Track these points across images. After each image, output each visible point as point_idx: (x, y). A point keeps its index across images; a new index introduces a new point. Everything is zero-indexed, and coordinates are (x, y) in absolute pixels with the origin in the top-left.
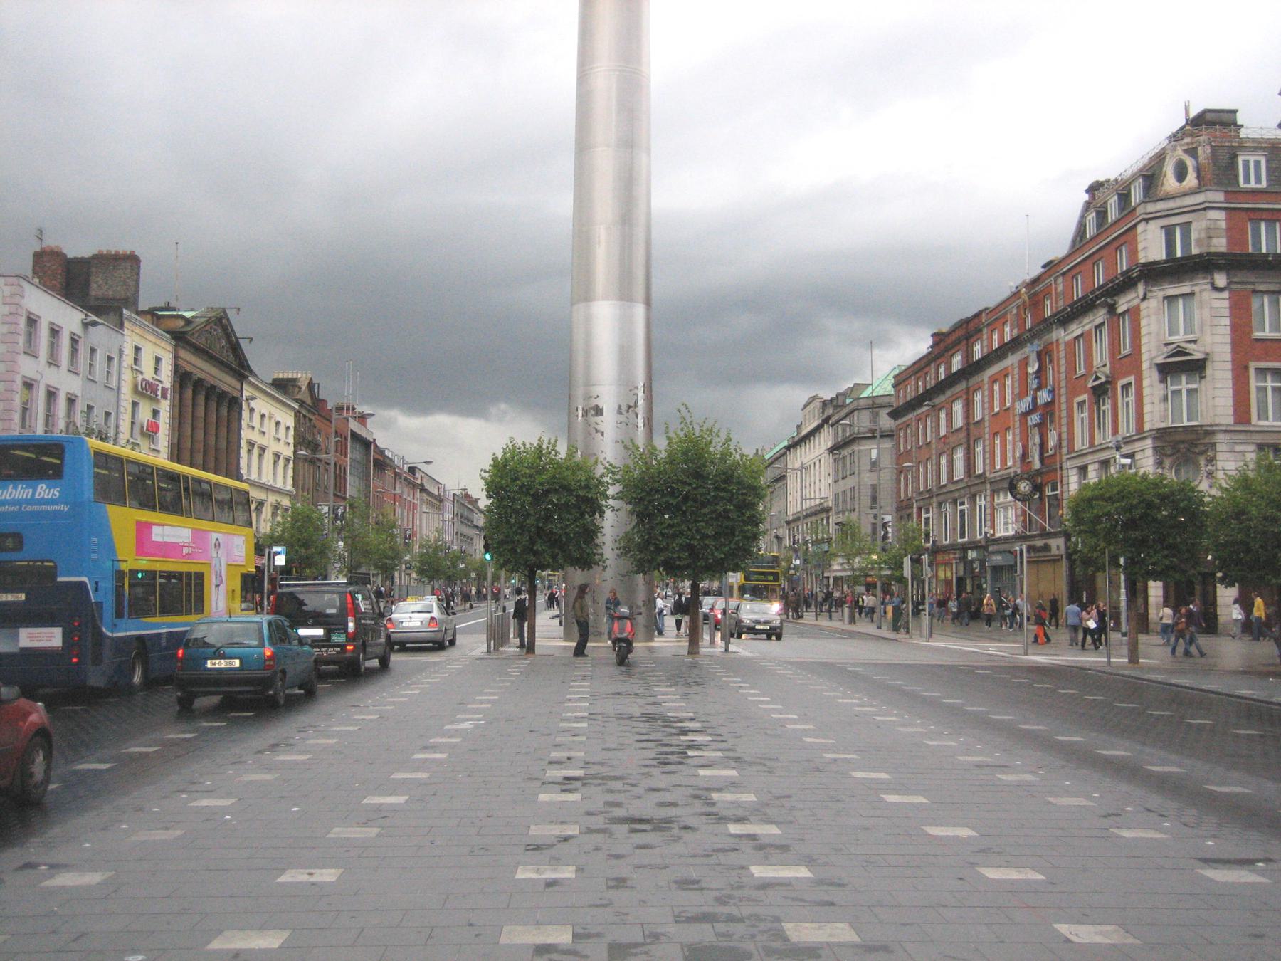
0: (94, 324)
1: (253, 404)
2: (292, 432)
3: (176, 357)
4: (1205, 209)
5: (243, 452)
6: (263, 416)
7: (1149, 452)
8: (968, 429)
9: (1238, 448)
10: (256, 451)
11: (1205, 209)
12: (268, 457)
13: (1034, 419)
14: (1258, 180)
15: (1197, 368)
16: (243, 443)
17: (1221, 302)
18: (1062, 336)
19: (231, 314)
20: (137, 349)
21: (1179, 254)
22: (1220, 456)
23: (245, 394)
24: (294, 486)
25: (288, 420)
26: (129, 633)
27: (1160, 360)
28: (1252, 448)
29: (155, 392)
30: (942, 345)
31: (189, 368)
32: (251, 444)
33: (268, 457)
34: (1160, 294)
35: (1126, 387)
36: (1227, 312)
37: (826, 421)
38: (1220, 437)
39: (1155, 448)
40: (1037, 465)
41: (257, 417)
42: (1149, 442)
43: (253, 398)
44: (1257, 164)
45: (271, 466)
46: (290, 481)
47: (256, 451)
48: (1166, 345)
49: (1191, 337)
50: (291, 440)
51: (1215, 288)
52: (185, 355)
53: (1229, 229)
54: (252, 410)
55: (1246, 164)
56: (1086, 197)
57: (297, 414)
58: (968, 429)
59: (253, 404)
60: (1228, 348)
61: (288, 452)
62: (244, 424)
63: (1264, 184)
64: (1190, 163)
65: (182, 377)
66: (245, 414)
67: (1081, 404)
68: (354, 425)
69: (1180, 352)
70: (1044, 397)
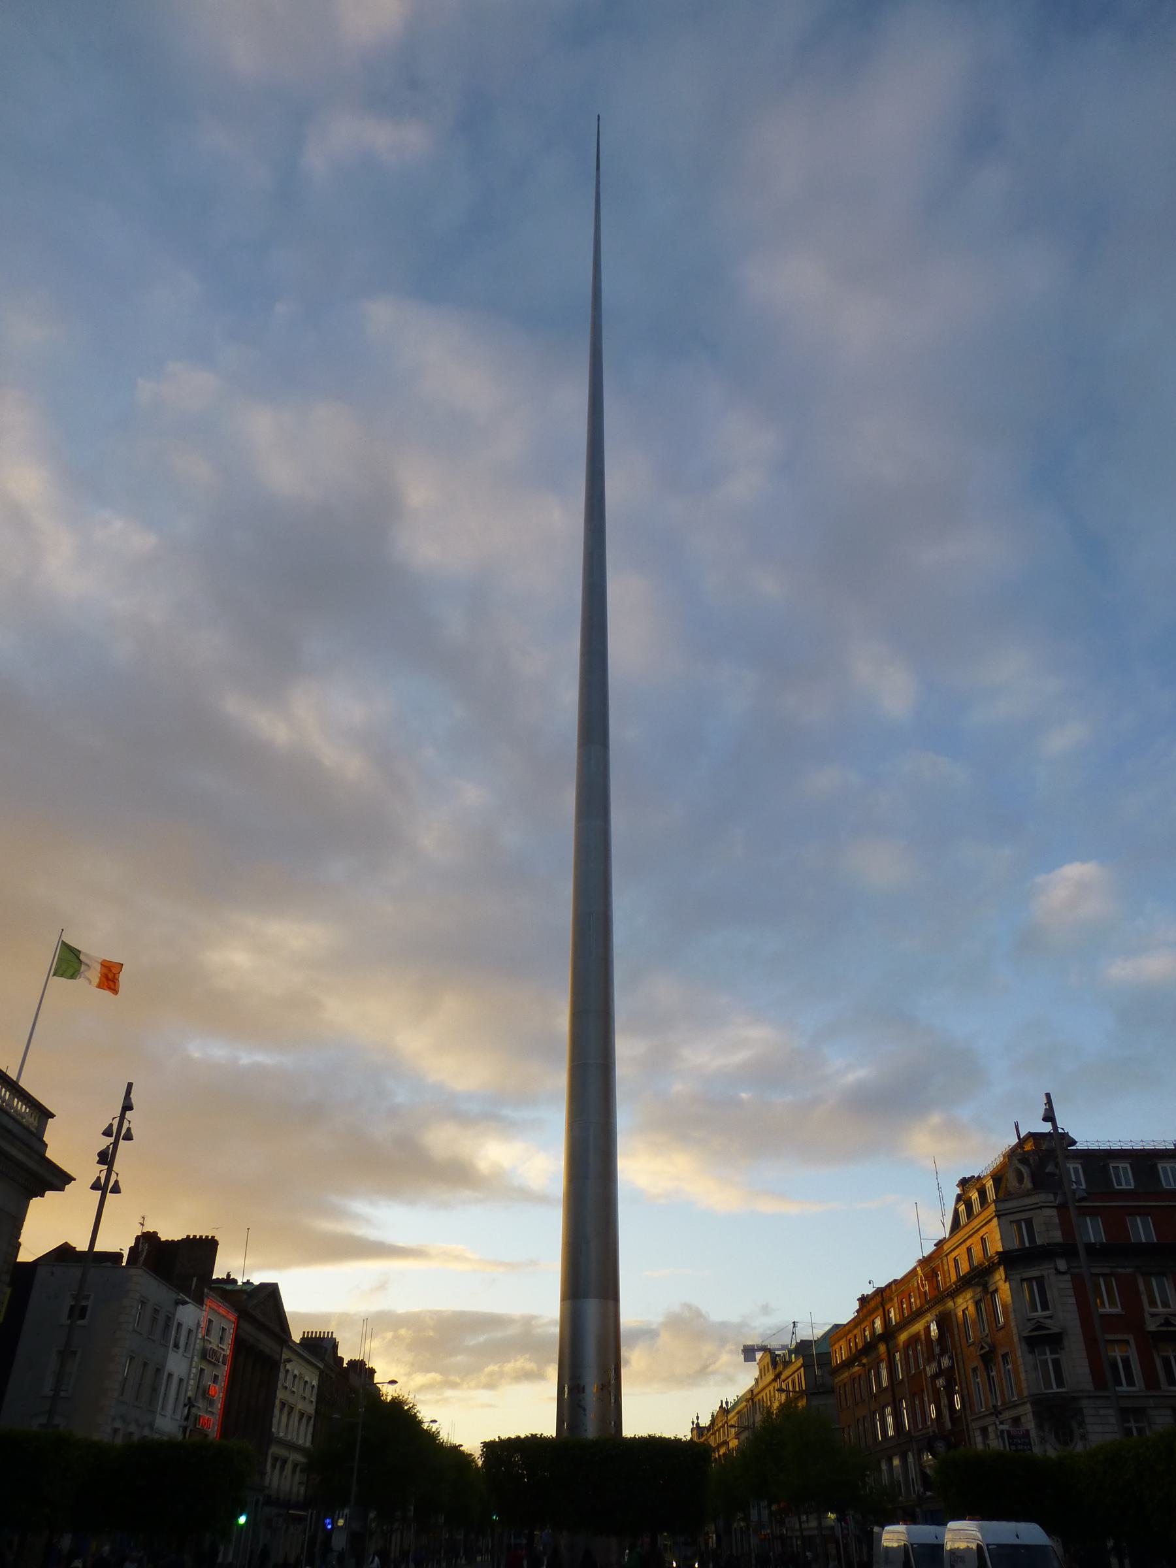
1: (289, 1366)
2: (315, 1391)
3: (237, 1328)
4: (1041, 1208)
5: (276, 1411)
6: (295, 1376)
7: (1030, 1416)
8: (893, 1391)
9: (1102, 1412)
11: (1041, 1208)
12: (295, 1416)
13: (941, 1382)
15: (1055, 1341)
16: (277, 1403)
17: (1065, 1283)
20: (210, 1321)
21: (1027, 1245)
23: (284, 1356)
27: (1026, 1334)
29: (218, 1360)
30: (865, 1310)
32: (283, 1404)
33: (295, 1416)
34: (1018, 1277)
35: (1005, 1356)
36: (1071, 1292)
37: (778, 1376)
38: (1084, 1403)
40: (949, 1425)
41: (290, 1377)
42: (1028, 1406)
43: (289, 1361)
45: (296, 1423)
46: (309, 1437)
47: (286, 1410)
48: (1029, 1320)
49: (1047, 1313)
50: (314, 1399)
51: (1059, 1272)
54: (287, 1371)
55: (1116, 1168)
56: (958, 1191)
57: (322, 1374)
58: (893, 1391)
59: (289, 1366)
60: (1078, 1323)
61: (311, 1409)
62: (279, 1385)
64: (1024, 1169)
65: (239, 1344)
66: (282, 1375)
67: (975, 1370)
69: (1040, 1327)
70: (946, 1362)
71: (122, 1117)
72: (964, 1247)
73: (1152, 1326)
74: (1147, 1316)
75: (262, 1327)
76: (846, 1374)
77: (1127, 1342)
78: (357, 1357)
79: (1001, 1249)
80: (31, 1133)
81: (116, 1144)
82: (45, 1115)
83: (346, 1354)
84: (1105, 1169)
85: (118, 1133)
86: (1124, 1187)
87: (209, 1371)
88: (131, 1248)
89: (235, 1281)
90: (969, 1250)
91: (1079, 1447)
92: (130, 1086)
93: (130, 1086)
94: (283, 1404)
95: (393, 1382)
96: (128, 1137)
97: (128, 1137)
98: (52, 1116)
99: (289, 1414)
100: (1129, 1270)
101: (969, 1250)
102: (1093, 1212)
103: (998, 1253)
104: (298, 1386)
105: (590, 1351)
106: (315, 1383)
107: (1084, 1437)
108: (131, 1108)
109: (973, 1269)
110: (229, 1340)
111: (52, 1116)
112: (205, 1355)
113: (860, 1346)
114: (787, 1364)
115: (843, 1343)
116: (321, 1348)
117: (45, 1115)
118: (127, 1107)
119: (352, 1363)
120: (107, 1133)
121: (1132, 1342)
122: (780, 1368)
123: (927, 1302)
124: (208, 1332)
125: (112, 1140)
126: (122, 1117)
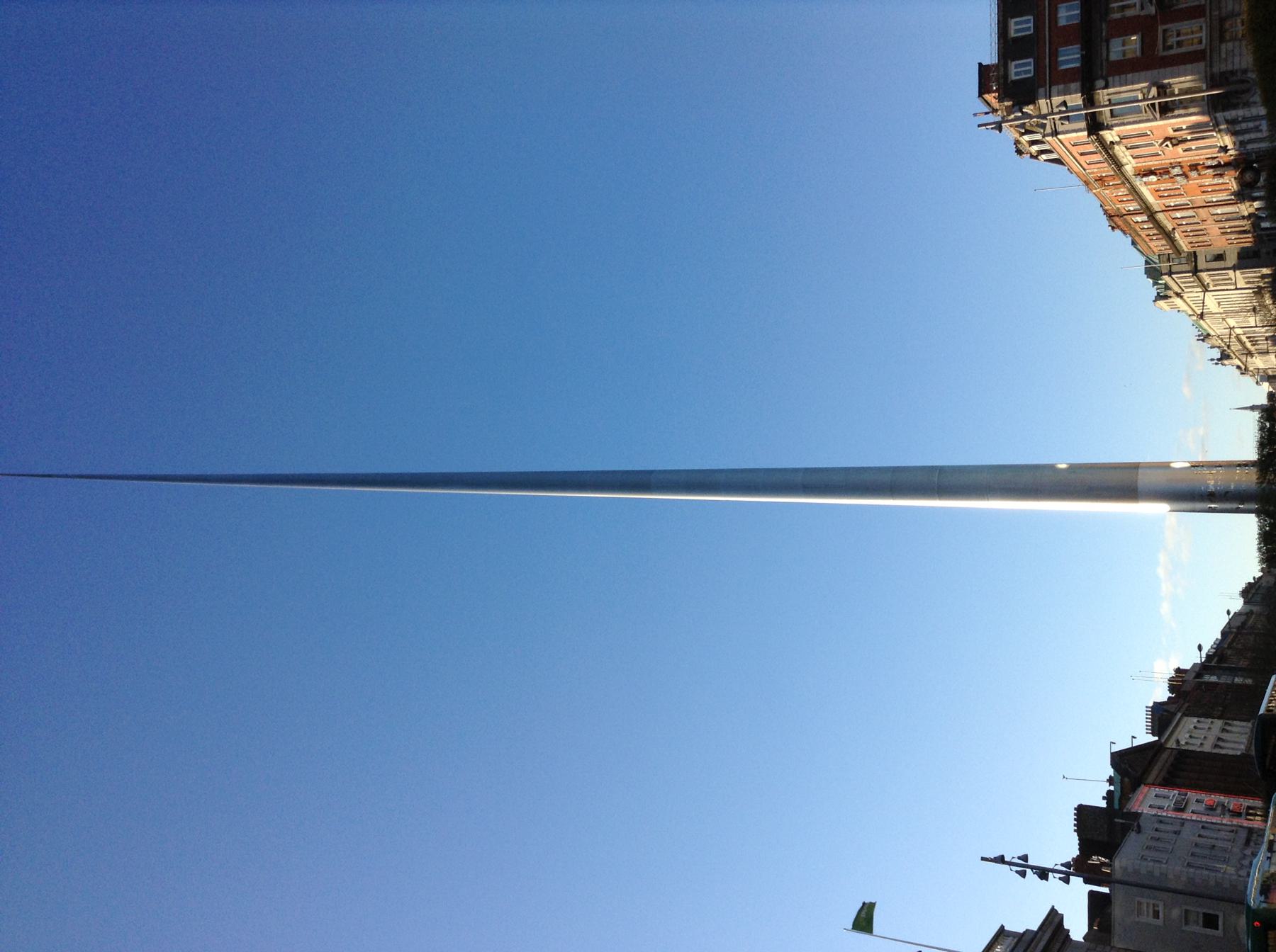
0: (1139, 826)
5: (1223, 752)
9: (1223, 56)
10: (1221, 744)
12: (1224, 736)
13: (1194, 174)
14: (1029, 64)
16: (1216, 751)
18: (1129, 169)
19: (1116, 748)
22: (1230, 67)
23: (1174, 746)
24: (1248, 720)
25: (1191, 722)
26: (351, 489)
27: (1158, 115)
28: (1223, 46)
31: (1163, 774)
32: (1216, 746)
33: (1224, 736)
37: (1178, 295)
38: (1215, 70)
39: (1223, 110)
43: (1178, 742)
44: (1016, 23)
47: (1221, 744)
52: (1150, 779)
53: (1064, 83)
55: (1017, 74)
57: (1185, 715)
61: (1219, 723)
63: (1031, 18)
65: (1167, 782)
66: (1191, 748)
68: (1190, 677)
71: (1010, 864)
72: (1079, 157)
73: (1152, 10)
74: (1143, 13)
75: (1152, 762)
76: (1181, 242)
77: (1165, 31)
78: (1166, 686)
79: (1086, 133)
80: (1017, 944)
81: (1032, 868)
82: (1002, 933)
83: (1163, 694)
84: (1015, 40)
85: (1023, 866)
86: (1031, 25)
87: (1193, 806)
88: (1086, 882)
89: (1109, 792)
90: (1082, 154)
91: (1252, 75)
92: (983, 859)
93: (983, 859)
94: (1216, 746)
95: (1200, 648)
96: (1025, 858)
97: (1025, 858)
98: (1002, 927)
99: (1223, 740)
100: (1104, 26)
101: (1082, 154)
102: (1054, 55)
103: (1089, 135)
104: (1195, 734)
105: (1200, 493)
106: (1195, 720)
107: (1245, 71)
108: (1003, 857)
109: (1131, 193)
110: (1165, 791)
111: (1002, 927)
112: (1179, 809)
113: (1155, 232)
114: (1167, 287)
115: (1152, 244)
116: (1161, 717)
117: (1002, 933)
118: (1001, 860)
119: (1172, 688)
120: (1023, 874)
121: (1165, 27)
122: (1169, 293)
123: (1123, 183)
124: (1159, 808)
125: (1029, 871)
126: (1010, 864)
